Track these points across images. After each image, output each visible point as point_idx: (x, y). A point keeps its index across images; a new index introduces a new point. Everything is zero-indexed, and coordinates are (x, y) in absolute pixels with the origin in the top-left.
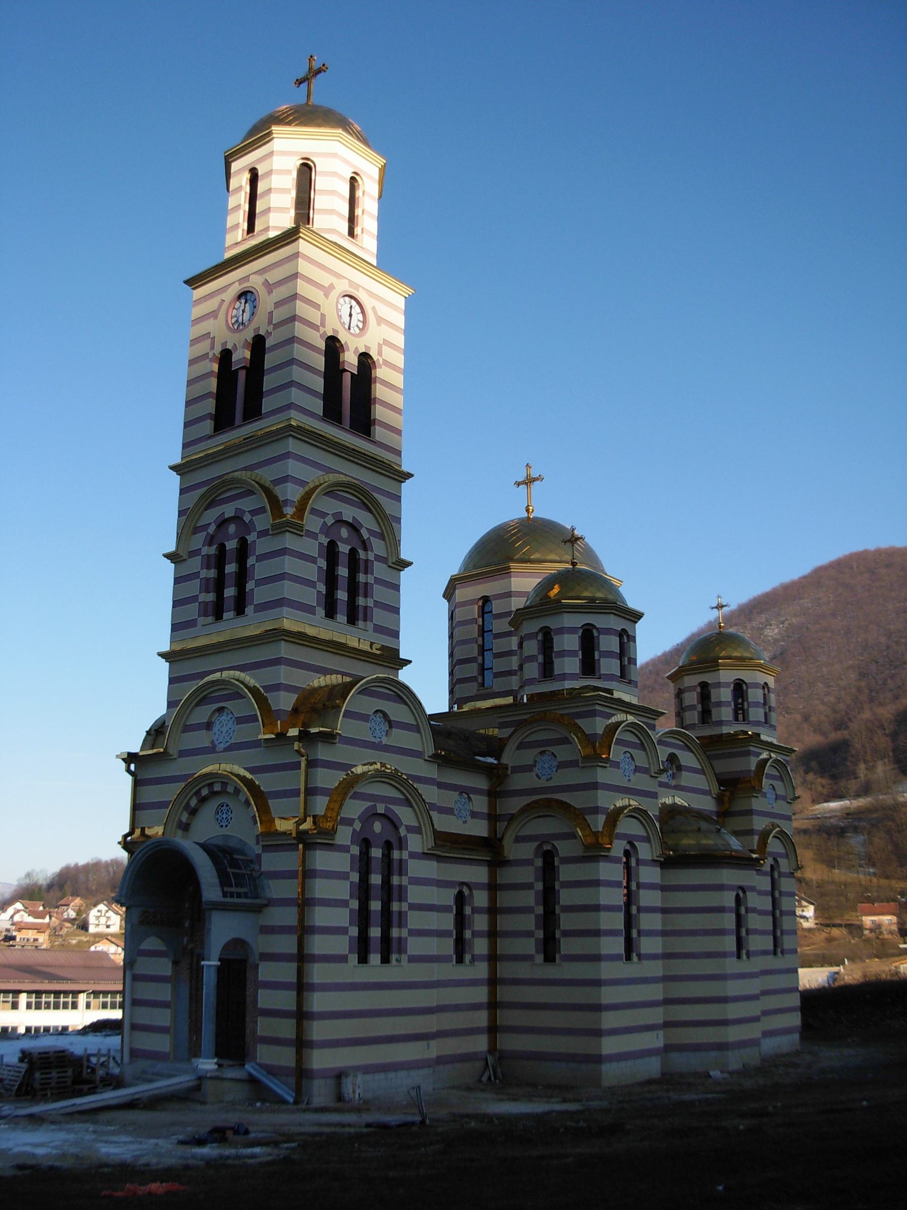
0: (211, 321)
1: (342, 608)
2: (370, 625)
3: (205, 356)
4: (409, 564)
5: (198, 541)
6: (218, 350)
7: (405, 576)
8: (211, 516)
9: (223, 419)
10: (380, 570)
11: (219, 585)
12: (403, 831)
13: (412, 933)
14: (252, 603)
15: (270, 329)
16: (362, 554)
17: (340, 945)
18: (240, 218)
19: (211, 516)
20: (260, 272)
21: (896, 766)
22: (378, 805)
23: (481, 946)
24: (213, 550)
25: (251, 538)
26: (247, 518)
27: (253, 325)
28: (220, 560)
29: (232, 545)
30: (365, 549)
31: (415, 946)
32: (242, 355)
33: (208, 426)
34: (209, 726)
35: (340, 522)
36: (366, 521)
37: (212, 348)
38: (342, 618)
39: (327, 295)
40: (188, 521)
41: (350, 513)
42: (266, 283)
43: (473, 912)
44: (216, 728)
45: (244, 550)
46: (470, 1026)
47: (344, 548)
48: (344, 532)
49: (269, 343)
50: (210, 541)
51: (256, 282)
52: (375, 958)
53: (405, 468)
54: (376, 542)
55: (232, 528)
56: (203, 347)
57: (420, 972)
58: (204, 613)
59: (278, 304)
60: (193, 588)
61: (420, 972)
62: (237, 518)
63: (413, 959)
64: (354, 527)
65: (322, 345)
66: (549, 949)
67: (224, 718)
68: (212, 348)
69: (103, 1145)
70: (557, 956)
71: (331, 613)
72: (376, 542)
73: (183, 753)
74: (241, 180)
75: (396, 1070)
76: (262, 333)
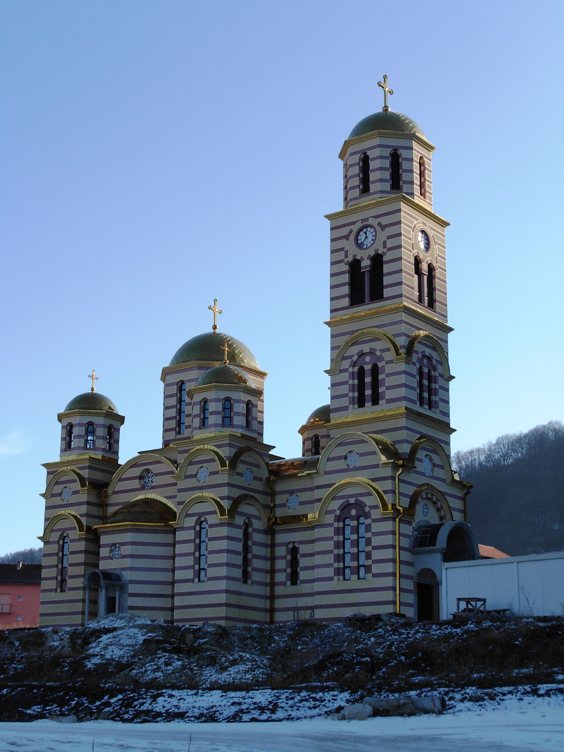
1: (426, 401)
2: (438, 411)
3: (342, 261)
4: (454, 377)
5: (346, 364)
6: (350, 259)
7: (452, 383)
8: (354, 351)
9: (356, 298)
10: (441, 381)
11: (361, 387)
13: (331, 552)
15: (385, 250)
16: (433, 373)
19: (354, 351)
20: (376, 217)
21: (522, 436)
23: (281, 551)
24: (356, 369)
25: (380, 365)
26: (378, 353)
27: (375, 247)
28: (361, 374)
29: (368, 367)
30: (434, 370)
33: (346, 302)
34: (345, 458)
35: (424, 356)
36: (435, 356)
37: (346, 256)
38: (427, 407)
40: (339, 354)
41: (428, 351)
44: (349, 459)
45: (375, 371)
46: (240, 597)
47: (426, 370)
48: (425, 361)
49: (385, 258)
50: (354, 364)
53: (449, 324)
54: (439, 366)
55: (368, 359)
56: (341, 256)
58: (352, 401)
59: (389, 237)
60: (345, 389)
62: (372, 353)
64: (429, 359)
65: (412, 261)
67: (352, 454)
71: (421, 404)
72: (439, 366)
73: (327, 473)
76: (380, 252)
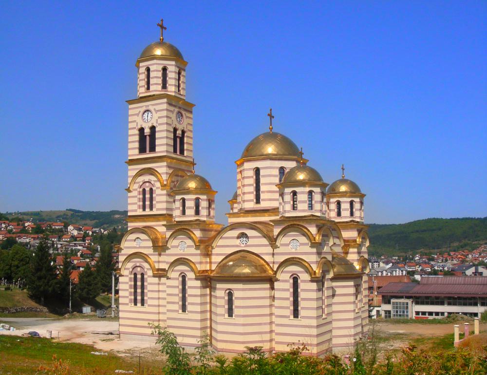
0: (136, 116)
12: (146, 270)
14: (155, 207)
15: (157, 125)
17: (126, 301)
18: (143, 83)
22: (99, 253)
24: (141, 190)
25: (154, 188)
27: (152, 122)
29: (147, 189)
31: (150, 302)
32: (147, 131)
37: (137, 126)
39: (155, 109)
42: (155, 109)
43: (224, 306)
47: (147, 189)
49: (157, 129)
51: (151, 108)
52: (139, 305)
57: (242, 321)
61: (242, 321)
63: (149, 306)
66: (230, 312)
68: (137, 126)
69: (246, 352)
70: (234, 315)
74: (142, 70)
75: (263, 342)
